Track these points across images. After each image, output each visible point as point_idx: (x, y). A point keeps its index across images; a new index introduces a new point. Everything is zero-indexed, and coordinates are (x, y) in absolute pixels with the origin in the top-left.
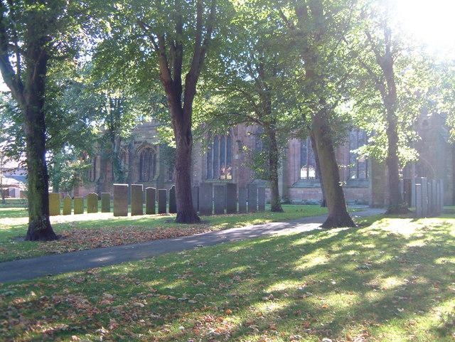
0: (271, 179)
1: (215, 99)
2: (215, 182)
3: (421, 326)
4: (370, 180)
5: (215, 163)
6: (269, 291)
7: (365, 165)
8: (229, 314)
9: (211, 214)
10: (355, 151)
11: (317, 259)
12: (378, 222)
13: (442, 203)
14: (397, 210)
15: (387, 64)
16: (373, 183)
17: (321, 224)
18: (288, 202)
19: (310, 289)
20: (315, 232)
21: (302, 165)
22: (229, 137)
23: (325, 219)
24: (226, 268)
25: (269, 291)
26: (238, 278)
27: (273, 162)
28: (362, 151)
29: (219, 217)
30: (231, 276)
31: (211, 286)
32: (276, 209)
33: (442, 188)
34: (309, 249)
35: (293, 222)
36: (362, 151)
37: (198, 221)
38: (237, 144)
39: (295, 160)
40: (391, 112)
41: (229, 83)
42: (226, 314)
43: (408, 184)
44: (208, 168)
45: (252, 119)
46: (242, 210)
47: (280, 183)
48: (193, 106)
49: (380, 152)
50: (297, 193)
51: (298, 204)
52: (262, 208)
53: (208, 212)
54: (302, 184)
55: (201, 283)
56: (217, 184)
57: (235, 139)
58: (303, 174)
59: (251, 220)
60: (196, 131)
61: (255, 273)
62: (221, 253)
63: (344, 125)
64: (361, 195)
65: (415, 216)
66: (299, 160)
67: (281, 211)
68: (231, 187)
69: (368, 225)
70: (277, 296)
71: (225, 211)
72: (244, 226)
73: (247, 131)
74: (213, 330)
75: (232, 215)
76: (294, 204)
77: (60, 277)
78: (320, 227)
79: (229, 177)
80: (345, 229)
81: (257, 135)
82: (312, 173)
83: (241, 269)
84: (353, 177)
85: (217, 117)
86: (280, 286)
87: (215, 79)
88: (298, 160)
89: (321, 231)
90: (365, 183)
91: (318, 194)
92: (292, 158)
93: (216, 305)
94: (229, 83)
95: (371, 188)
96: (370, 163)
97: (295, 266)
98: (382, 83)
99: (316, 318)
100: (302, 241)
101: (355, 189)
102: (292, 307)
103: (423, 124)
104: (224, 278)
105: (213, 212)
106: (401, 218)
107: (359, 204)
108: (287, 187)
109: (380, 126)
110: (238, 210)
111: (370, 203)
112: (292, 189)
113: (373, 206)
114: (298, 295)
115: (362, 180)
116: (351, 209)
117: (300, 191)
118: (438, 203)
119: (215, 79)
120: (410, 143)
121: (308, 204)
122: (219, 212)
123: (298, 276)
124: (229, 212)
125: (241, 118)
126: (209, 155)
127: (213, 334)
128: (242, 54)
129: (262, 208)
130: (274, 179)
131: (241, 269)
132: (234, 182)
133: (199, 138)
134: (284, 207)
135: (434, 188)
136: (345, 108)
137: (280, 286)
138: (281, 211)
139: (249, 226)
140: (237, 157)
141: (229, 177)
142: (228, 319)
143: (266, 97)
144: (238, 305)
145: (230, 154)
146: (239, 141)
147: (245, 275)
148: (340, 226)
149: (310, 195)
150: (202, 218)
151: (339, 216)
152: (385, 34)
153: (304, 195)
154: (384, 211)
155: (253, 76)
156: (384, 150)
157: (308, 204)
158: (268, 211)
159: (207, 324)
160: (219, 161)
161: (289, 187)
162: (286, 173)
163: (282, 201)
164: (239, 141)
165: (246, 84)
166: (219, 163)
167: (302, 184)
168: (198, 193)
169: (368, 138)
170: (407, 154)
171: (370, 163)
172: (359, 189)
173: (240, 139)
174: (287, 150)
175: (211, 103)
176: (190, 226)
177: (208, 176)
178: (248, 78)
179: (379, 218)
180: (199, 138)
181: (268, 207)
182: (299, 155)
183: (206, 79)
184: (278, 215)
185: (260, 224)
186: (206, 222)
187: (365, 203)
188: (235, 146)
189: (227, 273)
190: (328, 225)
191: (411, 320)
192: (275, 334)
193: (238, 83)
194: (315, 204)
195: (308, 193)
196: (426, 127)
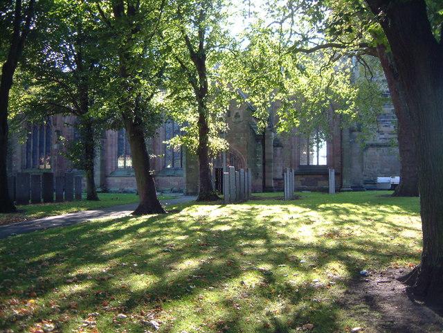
0: (87, 169)
1: (33, 89)
2: (32, 171)
3: (208, 300)
4: (185, 169)
5: (34, 152)
6: (74, 274)
7: (180, 155)
8: (35, 297)
9: (28, 203)
10: (167, 142)
11: (122, 244)
12: (187, 208)
13: (250, 191)
14: (208, 196)
15: (199, 58)
16: (187, 172)
17: (132, 212)
18: (105, 191)
19: (114, 271)
20: (125, 220)
21: (119, 155)
22: (48, 127)
23: (137, 206)
24: (31, 255)
25: (74, 274)
26: (48, 263)
27: (90, 152)
28: (175, 142)
29: (36, 206)
30: (40, 262)
31: (20, 272)
32: (92, 197)
33: (250, 177)
34: (117, 235)
35: (107, 209)
36: (175, 142)
37: (15, 211)
38: (55, 133)
39: (111, 150)
40: (202, 105)
41: (46, 73)
42: (30, 297)
43: (219, 172)
44: (27, 158)
45: (69, 110)
46: (59, 199)
47: (97, 173)
48: (10, 96)
49: (192, 142)
50: (114, 181)
51: (116, 192)
52: (79, 197)
53: (25, 202)
54: (119, 173)
55: (10, 269)
56: (33, 174)
57: (54, 129)
58: (121, 163)
59: (67, 208)
60: (13, 121)
61: (63, 258)
62: (33, 240)
63: (156, 117)
64: (176, 183)
65: (223, 203)
66: (117, 150)
67: (97, 199)
68: (48, 175)
69: (177, 211)
70: (81, 279)
71: (42, 200)
72: (59, 214)
73: (66, 122)
74: (17, 312)
75: (48, 204)
76: (111, 192)
77: (31, 260)
78: (132, 214)
79: (48, 166)
80: (155, 215)
81: (76, 125)
82: (129, 163)
83: (51, 255)
84: (169, 167)
85: (34, 107)
86: (85, 270)
87: (32, 69)
88: (115, 149)
89: (132, 217)
90: (179, 172)
91: (133, 184)
92: (109, 148)
93: (21, 289)
94: (46, 73)
95: (185, 176)
96: (184, 153)
97: (102, 251)
98: (194, 76)
99: (114, 296)
100: (111, 228)
101: (171, 178)
102: (93, 288)
103: (235, 116)
104: (33, 264)
105: (30, 201)
106: (209, 204)
107: (175, 192)
108: (104, 176)
109: (193, 118)
110: (55, 199)
111: (185, 191)
112: (110, 178)
113: (187, 194)
114: (101, 280)
115: (177, 169)
116: (163, 198)
117: (117, 180)
118: (246, 191)
119: (32, 69)
120: (221, 134)
121: (125, 192)
122: (36, 201)
123: (102, 260)
124: (45, 202)
125: (59, 108)
126: (28, 144)
127: (16, 316)
128: (62, 46)
129: (79, 197)
130: (89, 168)
131: (51, 255)
132: (52, 171)
133: (17, 128)
134: (100, 196)
135: (242, 177)
136: (160, 99)
137: (85, 270)
138: (97, 199)
139: (64, 215)
140: (55, 147)
141: (48, 166)
142: (32, 301)
143: (83, 89)
144: (43, 289)
145: (48, 144)
146: (57, 131)
147: (53, 261)
148: (150, 213)
149: (127, 184)
150: (20, 207)
151: (149, 204)
152: (199, 32)
153: (121, 184)
154: (195, 198)
155: (71, 68)
156: (196, 141)
157: (125, 192)
158: (84, 200)
159: (12, 306)
160: (38, 149)
161: (107, 177)
162: (104, 162)
163: (99, 190)
164: (57, 131)
165: (65, 76)
166: (38, 153)
167: (119, 173)
168: (15, 183)
169: (179, 128)
170: (217, 143)
171: (184, 153)
172: (174, 178)
173: (59, 128)
174: (104, 140)
175: (29, 93)
176: (6, 215)
177: (28, 166)
178: (67, 70)
179: (189, 205)
180: (17, 128)
181: (84, 196)
182: (117, 145)
183: (23, 69)
184: (94, 203)
185: (76, 212)
186: (22, 211)
187: (181, 191)
188: (54, 135)
189: (36, 259)
190: (138, 213)
191: (200, 295)
192: (75, 313)
193: (58, 73)
194: (132, 192)
195: (125, 182)
196: (238, 120)
